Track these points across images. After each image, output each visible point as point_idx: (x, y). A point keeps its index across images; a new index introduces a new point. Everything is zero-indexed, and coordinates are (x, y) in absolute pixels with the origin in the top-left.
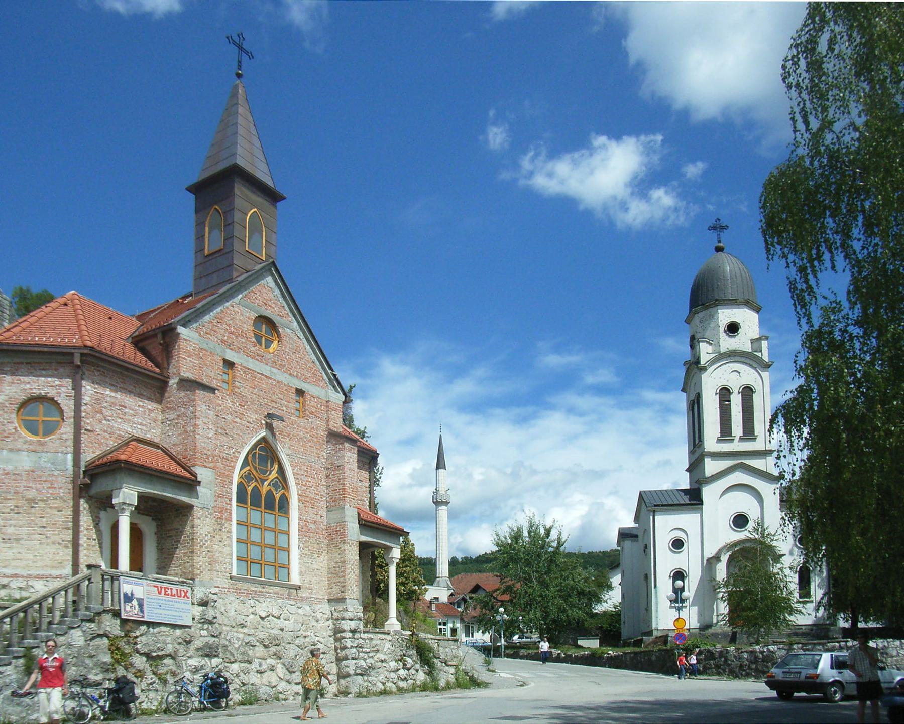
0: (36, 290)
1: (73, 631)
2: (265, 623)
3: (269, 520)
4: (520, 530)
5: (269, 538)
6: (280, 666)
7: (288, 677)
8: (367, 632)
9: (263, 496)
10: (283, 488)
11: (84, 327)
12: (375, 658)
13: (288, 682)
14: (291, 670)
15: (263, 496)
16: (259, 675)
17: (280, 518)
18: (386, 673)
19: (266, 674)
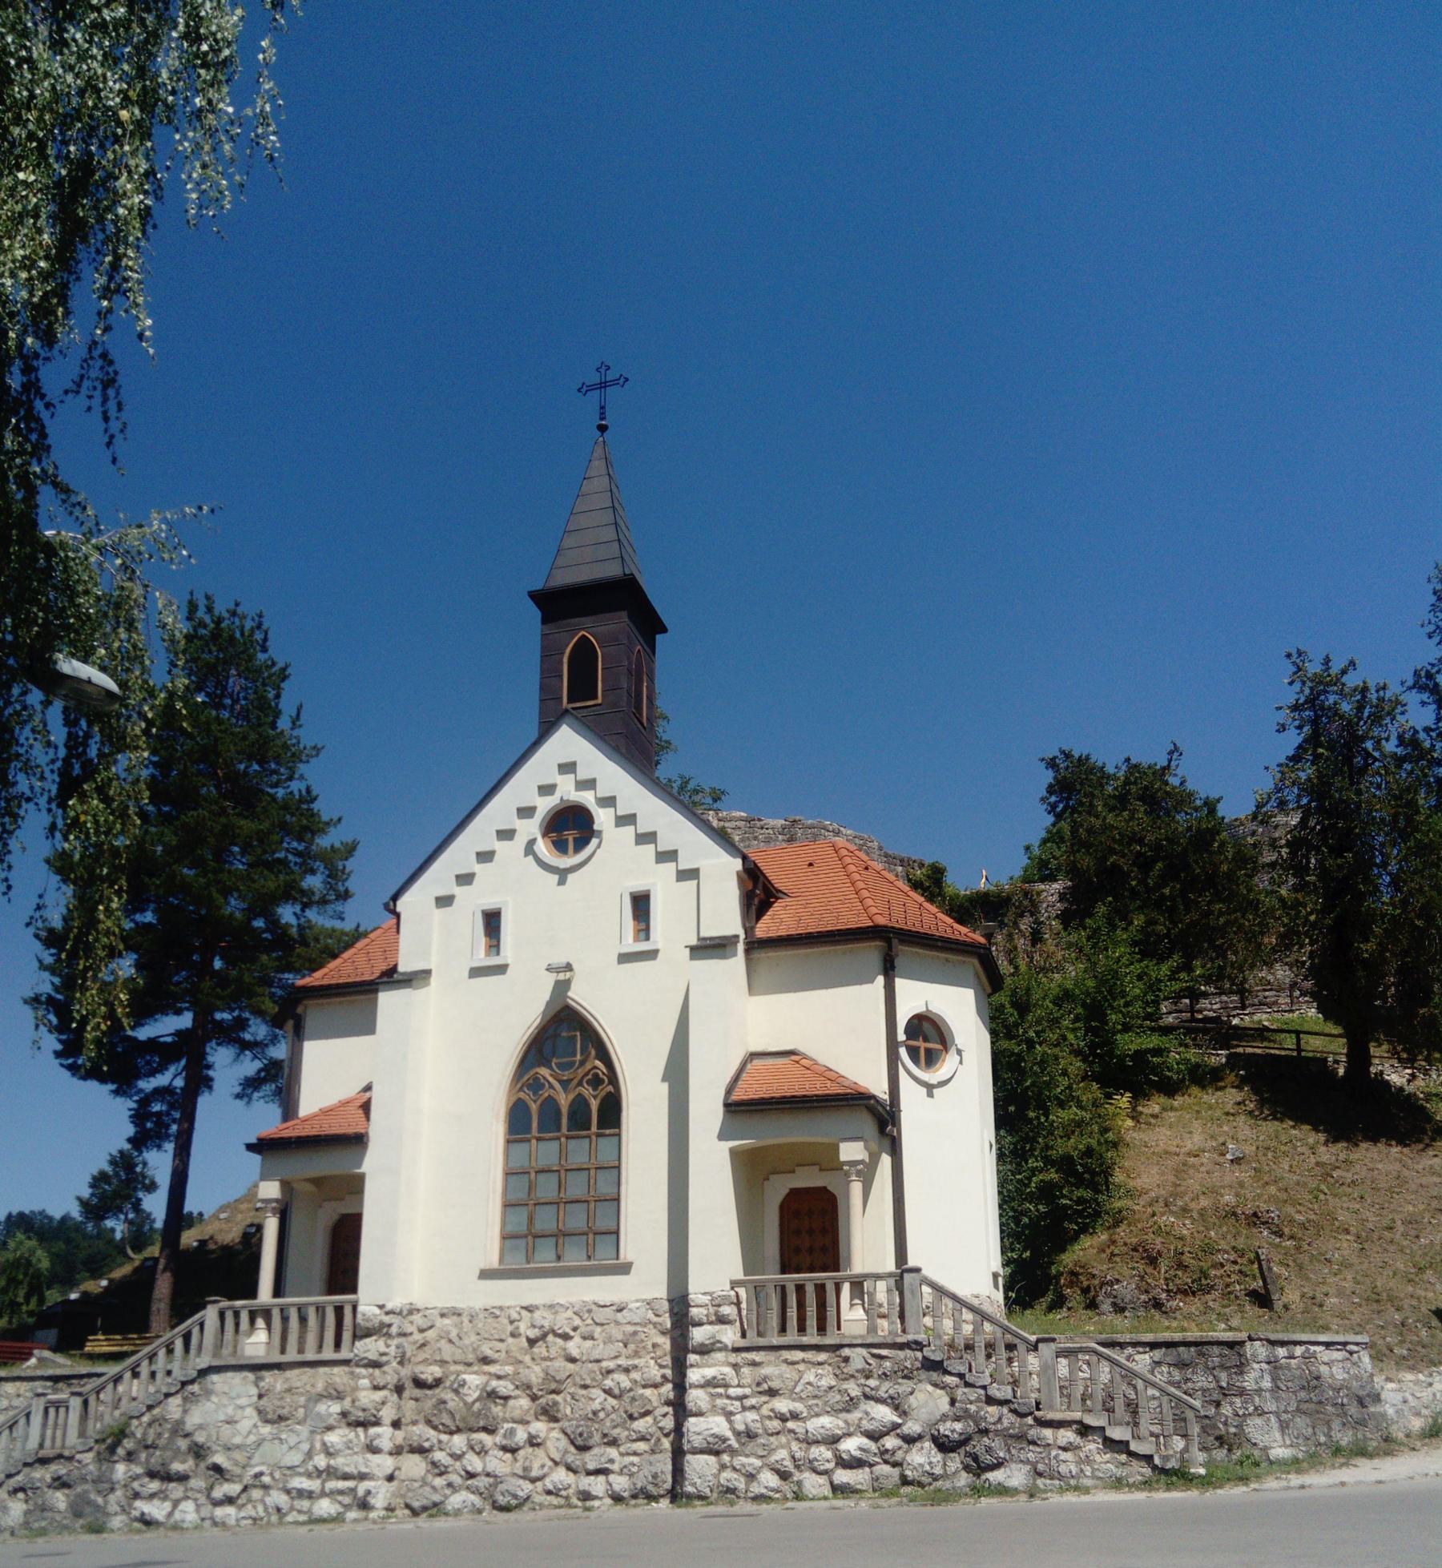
0: (37, 964)
1: (170, 1400)
2: (540, 1349)
3: (579, 1151)
4: (113, 1091)
5: (576, 1187)
6: (555, 1434)
7: (573, 1457)
8: (748, 1349)
9: (565, 1110)
10: (610, 1083)
11: (865, 893)
12: (765, 1411)
13: (569, 1468)
14: (579, 1441)
15: (565, 1110)
16: (509, 1455)
17: (572, 1143)
18: (795, 1446)
19: (521, 1452)
